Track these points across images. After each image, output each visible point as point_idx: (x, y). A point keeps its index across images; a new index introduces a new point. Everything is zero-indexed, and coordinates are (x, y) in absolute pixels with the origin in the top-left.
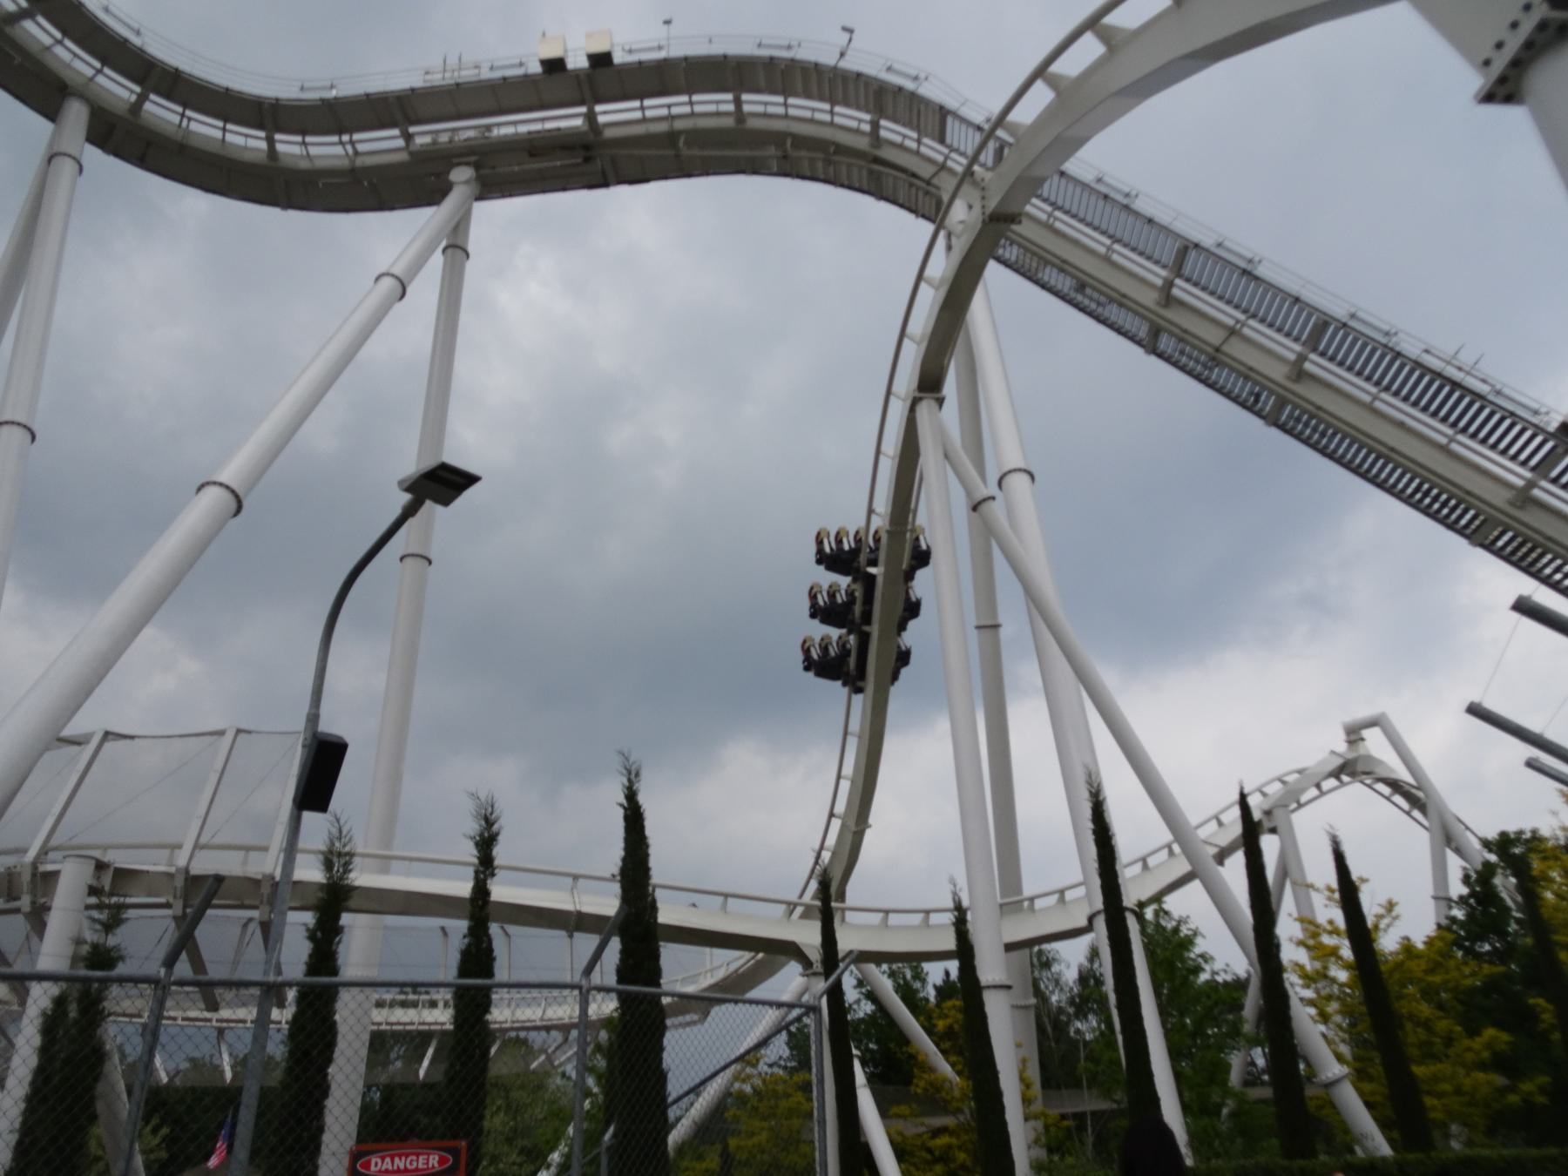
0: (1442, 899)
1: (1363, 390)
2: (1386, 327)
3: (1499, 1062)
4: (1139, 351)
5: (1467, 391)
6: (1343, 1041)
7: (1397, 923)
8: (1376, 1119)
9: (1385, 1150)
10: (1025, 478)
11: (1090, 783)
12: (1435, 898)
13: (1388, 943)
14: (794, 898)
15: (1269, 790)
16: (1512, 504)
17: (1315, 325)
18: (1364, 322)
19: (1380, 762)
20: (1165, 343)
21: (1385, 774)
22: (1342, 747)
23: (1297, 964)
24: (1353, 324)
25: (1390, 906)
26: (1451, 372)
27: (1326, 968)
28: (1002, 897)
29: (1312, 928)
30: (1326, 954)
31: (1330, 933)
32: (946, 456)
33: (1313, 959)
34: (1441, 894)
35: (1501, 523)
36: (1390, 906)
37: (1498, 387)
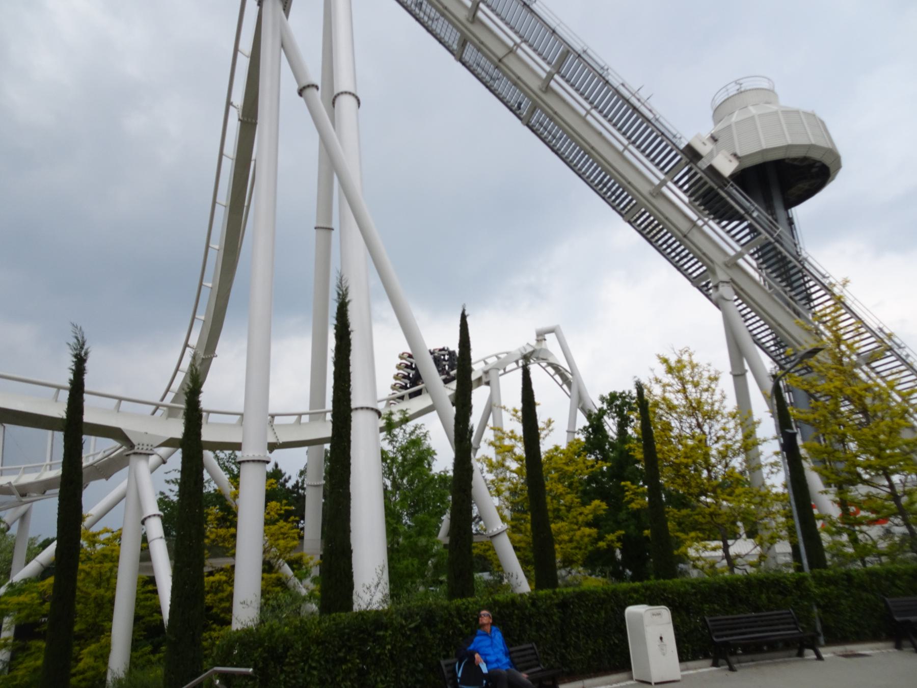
0: (571, 432)
1: (581, 105)
2: (602, 64)
3: (595, 523)
4: (451, 57)
5: (641, 115)
6: (507, 508)
7: (552, 434)
8: (519, 558)
9: (524, 586)
10: (353, 100)
11: (340, 287)
12: (568, 432)
13: (545, 446)
14: (157, 400)
15: (490, 361)
16: (651, 194)
17: (563, 52)
18: (590, 57)
19: (552, 354)
20: (470, 53)
21: (551, 360)
22: (533, 342)
23: (487, 458)
24: (584, 56)
25: (550, 422)
26: (633, 100)
27: (504, 460)
28: (205, 354)
29: (500, 434)
30: (504, 451)
31: (511, 438)
32: (282, 46)
33: (497, 453)
34: (571, 430)
35: (645, 206)
36: (550, 422)
37: (658, 116)
